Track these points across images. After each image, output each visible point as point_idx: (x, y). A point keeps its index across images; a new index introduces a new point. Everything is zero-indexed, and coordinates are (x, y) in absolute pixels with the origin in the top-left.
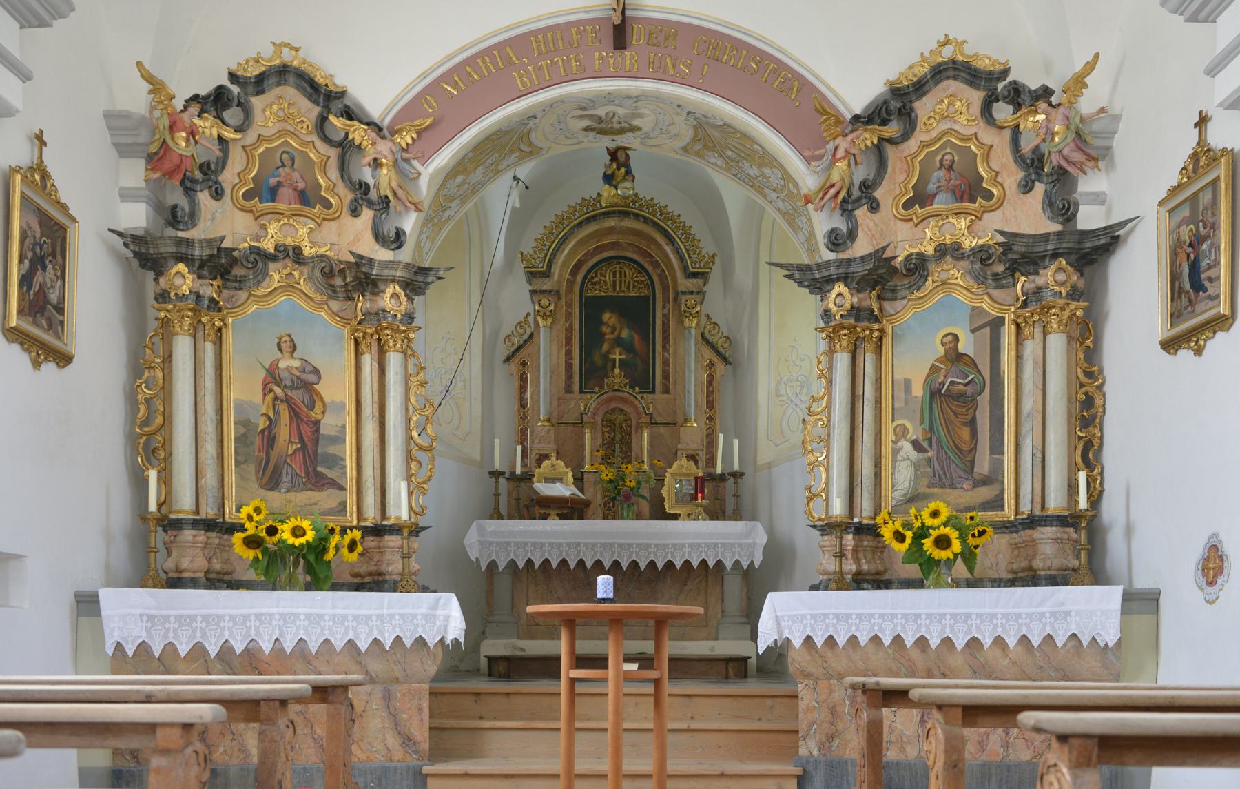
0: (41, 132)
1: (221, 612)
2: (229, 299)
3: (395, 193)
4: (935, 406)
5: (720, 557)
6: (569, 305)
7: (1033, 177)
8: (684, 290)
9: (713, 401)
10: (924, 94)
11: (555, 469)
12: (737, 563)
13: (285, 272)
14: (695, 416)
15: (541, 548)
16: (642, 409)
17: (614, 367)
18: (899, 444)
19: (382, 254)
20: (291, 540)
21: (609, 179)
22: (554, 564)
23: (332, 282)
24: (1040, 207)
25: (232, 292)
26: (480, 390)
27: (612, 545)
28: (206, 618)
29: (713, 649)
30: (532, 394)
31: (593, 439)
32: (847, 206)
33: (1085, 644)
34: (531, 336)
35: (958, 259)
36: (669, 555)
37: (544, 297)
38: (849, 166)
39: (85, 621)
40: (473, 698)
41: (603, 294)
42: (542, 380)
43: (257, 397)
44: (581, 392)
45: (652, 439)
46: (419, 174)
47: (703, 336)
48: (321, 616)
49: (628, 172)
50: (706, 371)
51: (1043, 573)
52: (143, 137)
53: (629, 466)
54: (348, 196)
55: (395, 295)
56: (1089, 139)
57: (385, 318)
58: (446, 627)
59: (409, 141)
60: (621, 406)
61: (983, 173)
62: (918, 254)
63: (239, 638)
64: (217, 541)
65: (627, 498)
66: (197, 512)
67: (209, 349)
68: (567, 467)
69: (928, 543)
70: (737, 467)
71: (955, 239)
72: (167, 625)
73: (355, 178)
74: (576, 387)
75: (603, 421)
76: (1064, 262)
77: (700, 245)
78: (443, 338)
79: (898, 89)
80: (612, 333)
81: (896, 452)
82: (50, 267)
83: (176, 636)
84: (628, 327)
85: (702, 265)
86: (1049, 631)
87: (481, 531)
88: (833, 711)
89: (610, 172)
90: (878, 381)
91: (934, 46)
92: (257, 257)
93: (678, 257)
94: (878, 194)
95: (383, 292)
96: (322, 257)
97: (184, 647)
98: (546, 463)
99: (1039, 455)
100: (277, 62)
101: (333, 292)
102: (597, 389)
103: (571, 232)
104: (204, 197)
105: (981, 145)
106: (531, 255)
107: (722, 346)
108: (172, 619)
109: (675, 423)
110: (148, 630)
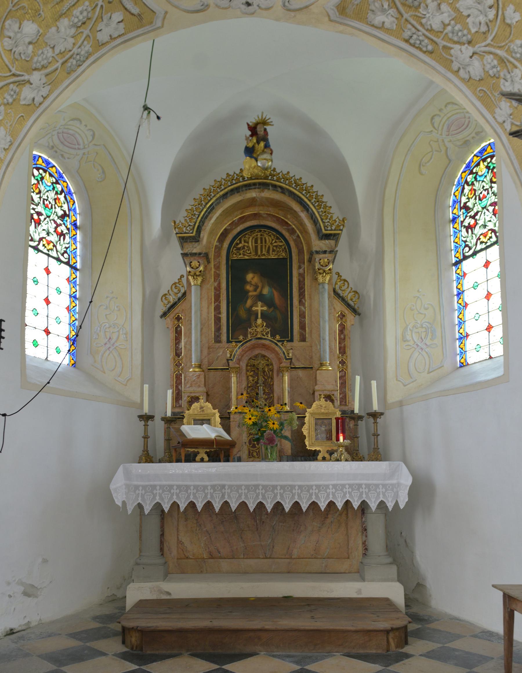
5: (364, 498)
6: (217, 267)
8: (318, 250)
9: (345, 347)
11: (203, 411)
12: (382, 503)
14: (330, 361)
15: (186, 491)
16: (282, 355)
17: (257, 318)
21: (250, 152)
29: (359, 591)
30: (186, 344)
31: (239, 382)
34: (184, 294)
36: (314, 497)
37: (195, 259)
41: (246, 257)
42: (193, 332)
44: (228, 341)
45: (291, 380)
47: (334, 291)
49: (267, 146)
50: (338, 321)
53: (272, 408)
60: (264, 353)
65: (271, 441)
68: (214, 409)
70: (376, 407)
74: (224, 338)
75: (247, 366)
78: (107, 297)
80: (255, 290)
84: (269, 285)
85: (333, 228)
87: (128, 475)
89: (250, 145)
93: (312, 222)
98: (195, 405)
102: (241, 338)
103: (218, 202)
106: (182, 223)
107: (351, 300)
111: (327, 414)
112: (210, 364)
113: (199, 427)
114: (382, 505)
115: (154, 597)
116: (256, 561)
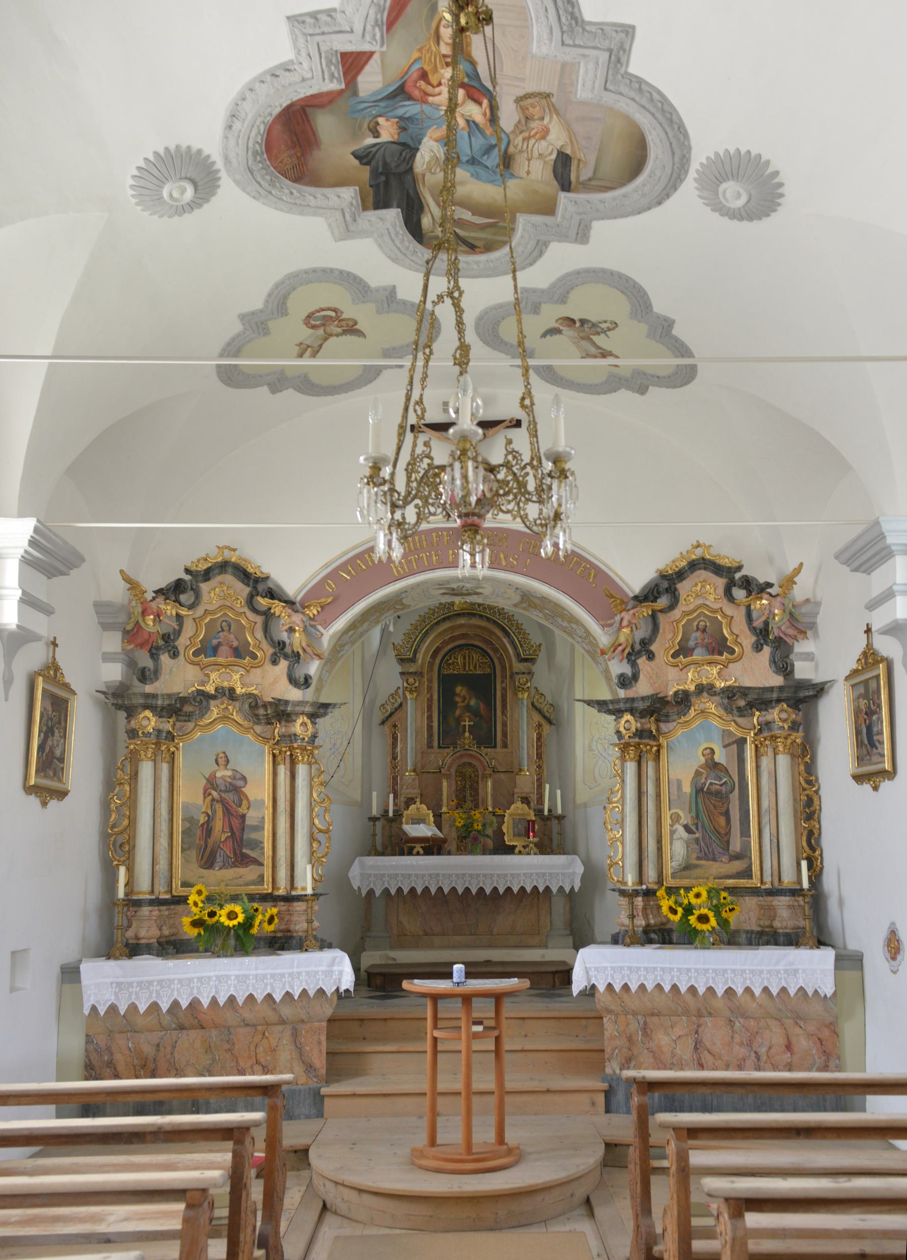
0: (55, 638)
1: (172, 977)
2: (180, 729)
3: (304, 650)
4: (699, 800)
5: (548, 883)
6: (430, 681)
7: (762, 641)
10: (684, 579)
13: (222, 707)
14: (528, 766)
17: (464, 731)
18: (675, 827)
19: (294, 694)
20: (227, 923)
22: (419, 891)
23: (257, 712)
24: (767, 663)
25: (182, 724)
26: (361, 749)
27: (464, 875)
28: (160, 982)
29: (543, 956)
30: (402, 749)
31: (449, 786)
32: (632, 657)
33: (810, 994)
34: (401, 705)
35: (712, 695)
38: (632, 630)
39: (67, 986)
40: (358, 1022)
43: (199, 800)
44: (439, 747)
46: (322, 635)
47: (533, 704)
48: (246, 976)
51: (781, 931)
52: (122, 618)
54: (270, 651)
55: (304, 724)
56: (799, 618)
57: (296, 740)
58: (340, 979)
59: (315, 612)
60: (470, 761)
61: (727, 635)
62: (683, 691)
63: (185, 997)
64: (167, 913)
65: (476, 839)
66: (152, 892)
67: (165, 767)
69: (692, 919)
70: (559, 811)
71: (709, 681)
72: (131, 990)
73: (276, 639)
74: (436, 744)
75: (456, 772)
76: (785, 706)
77: (530, 637)
79: (665, 576)
80: (463, 701)
81: (672, 833)
82: (57, 731)
83: (137, 998)
86: (783, 984)
87: (362, 866)
88: (630, 1039)
90: (658, 781)
91: (690, 548)
92: (202, 697)
94: (653, 648)
95: (295, 721)
96: (250, 695)
97: (143, 1005)
98: (412, 807)
99: (775, 840)
100: (220, 559)
101: (257, 719)
104: (165, 658)
105: (725, 616)
108: (135, 985)
109: (513, 771)
110: (116, 994)
111: (523, 815)
112: (423, 767)
113: (417, 826)
114: (561, 889)
115: (383, 962)
116: (464, 937)
